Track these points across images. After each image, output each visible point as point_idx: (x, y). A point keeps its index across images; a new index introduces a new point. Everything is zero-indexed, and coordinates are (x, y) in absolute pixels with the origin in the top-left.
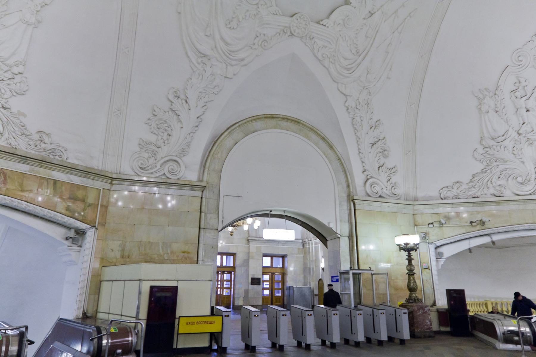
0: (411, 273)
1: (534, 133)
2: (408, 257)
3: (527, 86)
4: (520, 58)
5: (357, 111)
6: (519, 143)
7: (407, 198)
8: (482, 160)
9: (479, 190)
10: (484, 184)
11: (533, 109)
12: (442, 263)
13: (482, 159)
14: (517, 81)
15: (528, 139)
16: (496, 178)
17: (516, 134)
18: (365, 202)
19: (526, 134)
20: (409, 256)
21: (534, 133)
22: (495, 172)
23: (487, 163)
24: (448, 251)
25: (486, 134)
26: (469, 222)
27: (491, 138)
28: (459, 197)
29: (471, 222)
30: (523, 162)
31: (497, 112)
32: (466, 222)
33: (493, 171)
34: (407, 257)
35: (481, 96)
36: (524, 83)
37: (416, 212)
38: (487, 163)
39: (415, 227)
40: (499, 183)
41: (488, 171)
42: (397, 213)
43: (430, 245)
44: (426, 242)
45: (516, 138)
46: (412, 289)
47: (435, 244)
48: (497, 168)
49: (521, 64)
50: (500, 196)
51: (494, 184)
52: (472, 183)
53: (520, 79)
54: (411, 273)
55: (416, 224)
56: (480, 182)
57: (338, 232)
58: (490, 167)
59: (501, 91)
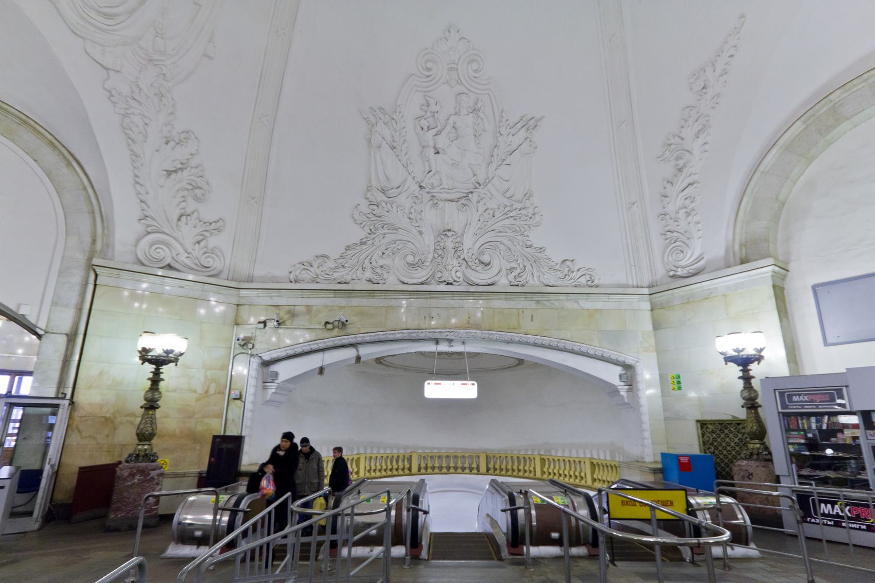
0: (151, 405)
1: (441, 189)
2: (153, 376)
3: (437, 112)
4: (429, 65)
5: (133, 103)
6: (419, 201)
7: (235, 277)
8: (364, 223)
9: (350, 272)
10: (360, 262)
11: (443, 150)
12: (274, 391)
13: (365, 221)
14: (425, 102)
15: (433, 196)
16: (378, 254)
17: (417, 186)
18: (122, 273)
19: (430, 189)
20: (157, 373)
21: (441, 189)
22: (379, 244)
23: (371, 230)
24: (286, 371)
25: (374, 183)
26: (323, 324)
27: (380, 189)
28: (318, 280)
29: (327, 323)
30: (421, 233)
31: (393, 148)
32: (319, 323)
33: (375, 243)
34: (151, 375)
35: (372, 119)
36: (433, 108)
37: (242, 301)
38: (371, 230)
39: (235, 327)
40: (382, 262)
41: (368, 243)
42: (199, 300)
43: (252, 359)
44: (248, 354)
45: (416, 194)
46: (144, 437)
47: (260, 357)
48: (384, 237)
49: (431, 75)
50: (378, 283)
51: (374, 264)
52: (342, 260)
53: (428, 99)
54: (151, 405)
55: (237, 321)
56: (354, 259)
57: (39, 325)
58: (373, 236)
59: (401, 115)
